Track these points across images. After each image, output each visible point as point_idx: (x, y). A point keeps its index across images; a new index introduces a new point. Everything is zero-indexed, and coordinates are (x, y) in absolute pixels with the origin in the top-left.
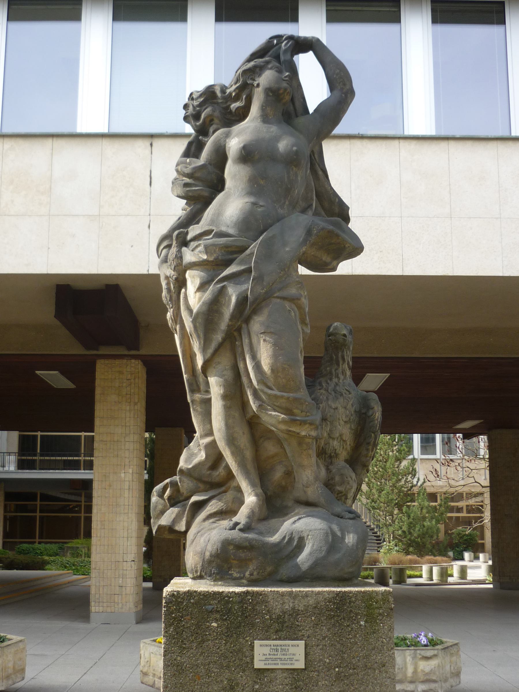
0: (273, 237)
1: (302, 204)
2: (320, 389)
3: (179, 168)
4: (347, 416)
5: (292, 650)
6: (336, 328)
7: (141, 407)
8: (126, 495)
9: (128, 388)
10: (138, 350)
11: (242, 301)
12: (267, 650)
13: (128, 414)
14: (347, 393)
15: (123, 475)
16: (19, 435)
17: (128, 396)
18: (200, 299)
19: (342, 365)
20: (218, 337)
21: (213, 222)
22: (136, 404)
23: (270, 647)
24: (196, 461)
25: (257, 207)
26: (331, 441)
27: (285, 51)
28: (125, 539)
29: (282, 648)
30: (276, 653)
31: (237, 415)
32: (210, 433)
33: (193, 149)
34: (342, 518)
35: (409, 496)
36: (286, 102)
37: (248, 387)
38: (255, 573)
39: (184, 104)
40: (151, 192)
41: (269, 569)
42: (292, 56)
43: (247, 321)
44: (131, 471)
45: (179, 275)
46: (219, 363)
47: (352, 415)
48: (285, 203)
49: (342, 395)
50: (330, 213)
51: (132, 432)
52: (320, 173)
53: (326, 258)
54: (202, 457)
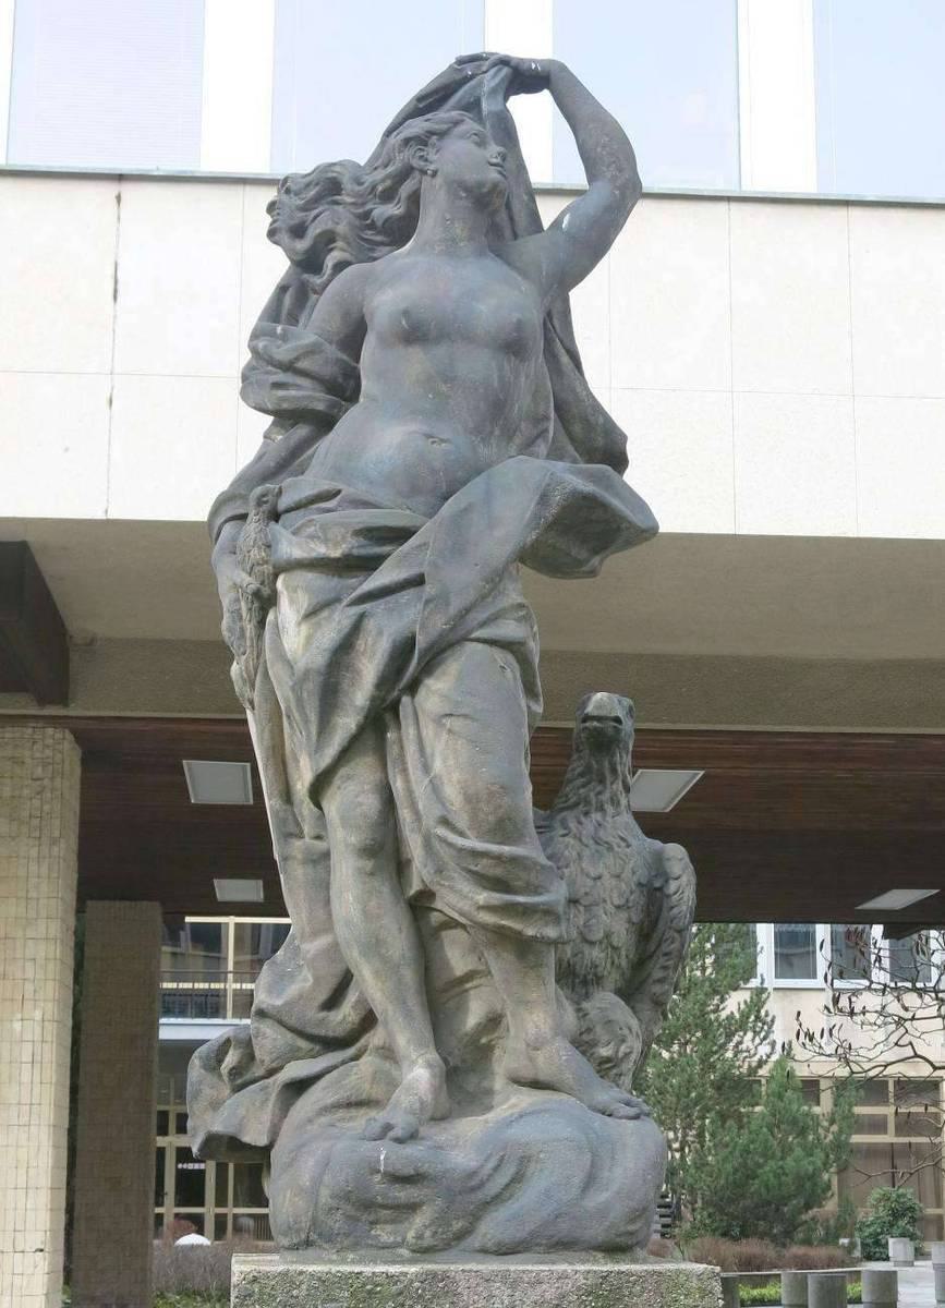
0: (467, 510)
1: (526, 429)
2: (564, 836)
3: (261, 345)
4: (621, 895)
6: (599, 706)
7: (65, 850)
8: (26, 1078)
9: (36, 803)
10: (66, 705)
11: (403, 651)
13: (33, 868)
14: (623, 844)
15: (17, 1026)
17: (36, 822)
18: (309, 639)
19: (612, 783)
20: (347, 723)
21: (338, 471)
22: (54, 842)
24: (293, 990)
25: (433, 442)
26: (586, 949)
27: (494, 91)
28: (22, 1193)
31: (386, 890)
32: (327, 926)
33: (288, 300)
34: (610, 1115)
35: (740, 1087)
36: (498, 210)
37: (412, 830)
39: (267, 203)
40: (115, 317)
41: (457, 1225)
42: (506, 99)
43: (413, 688)
44: (38, 1015)
45: (262, 583)
46: (349, 778)
47: (632, 893)
48: (492, 433)
49: (610, 848)
50: (591, 455)
51: (43, 913)
52: (565, 359)
53: (579, 552)
54: (305, 980)
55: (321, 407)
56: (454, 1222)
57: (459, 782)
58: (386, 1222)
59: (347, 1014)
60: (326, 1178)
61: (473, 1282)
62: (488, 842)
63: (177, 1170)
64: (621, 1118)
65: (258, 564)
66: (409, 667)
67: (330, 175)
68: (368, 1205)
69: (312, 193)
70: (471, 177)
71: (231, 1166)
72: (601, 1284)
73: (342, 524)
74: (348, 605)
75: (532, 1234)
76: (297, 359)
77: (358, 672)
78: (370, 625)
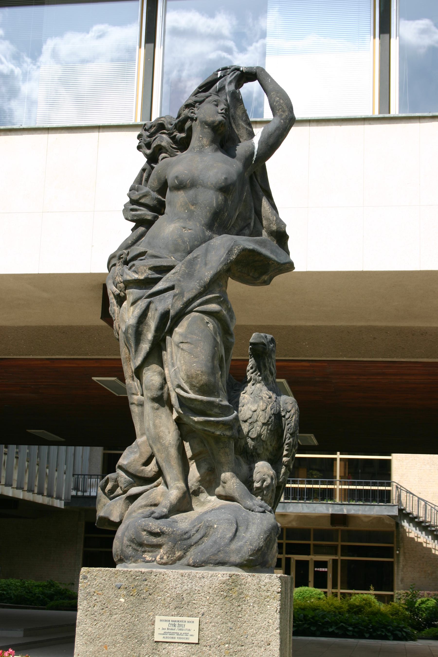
5: (188, 626)
11: (165, 316)
12: (166, 625)
16: (104, 454)
19: (264, 371)
20: (145, 347)
23: (168, 623)
25: (185, 230)
29: (180, 623)
30: (174, 628)
34: (252, 511)
38: (165, 557)
41: (178, 554)
43: (170, 332)
46: (148, 370)
55: (149, 218)
56: (177, 553)
57: (185, 370)
58: (149, 552)
59: (152, 468)
60: (126, 533)
61: (176, 576)
62: (198, 395)
63: (315, 571)
64: (256, 512)
65: (119, 283)
66: (168, 323)
67: (160, 122)
68: (141, 544)
69: (153, 130)
70: (210, 119)
71: (297, 456)
72: (229, 579)
73: (145, 266)
74: (145, 298)
75: (208, 558)
76: (140, 198)
77: (149, 326)
78: (152, 306)
